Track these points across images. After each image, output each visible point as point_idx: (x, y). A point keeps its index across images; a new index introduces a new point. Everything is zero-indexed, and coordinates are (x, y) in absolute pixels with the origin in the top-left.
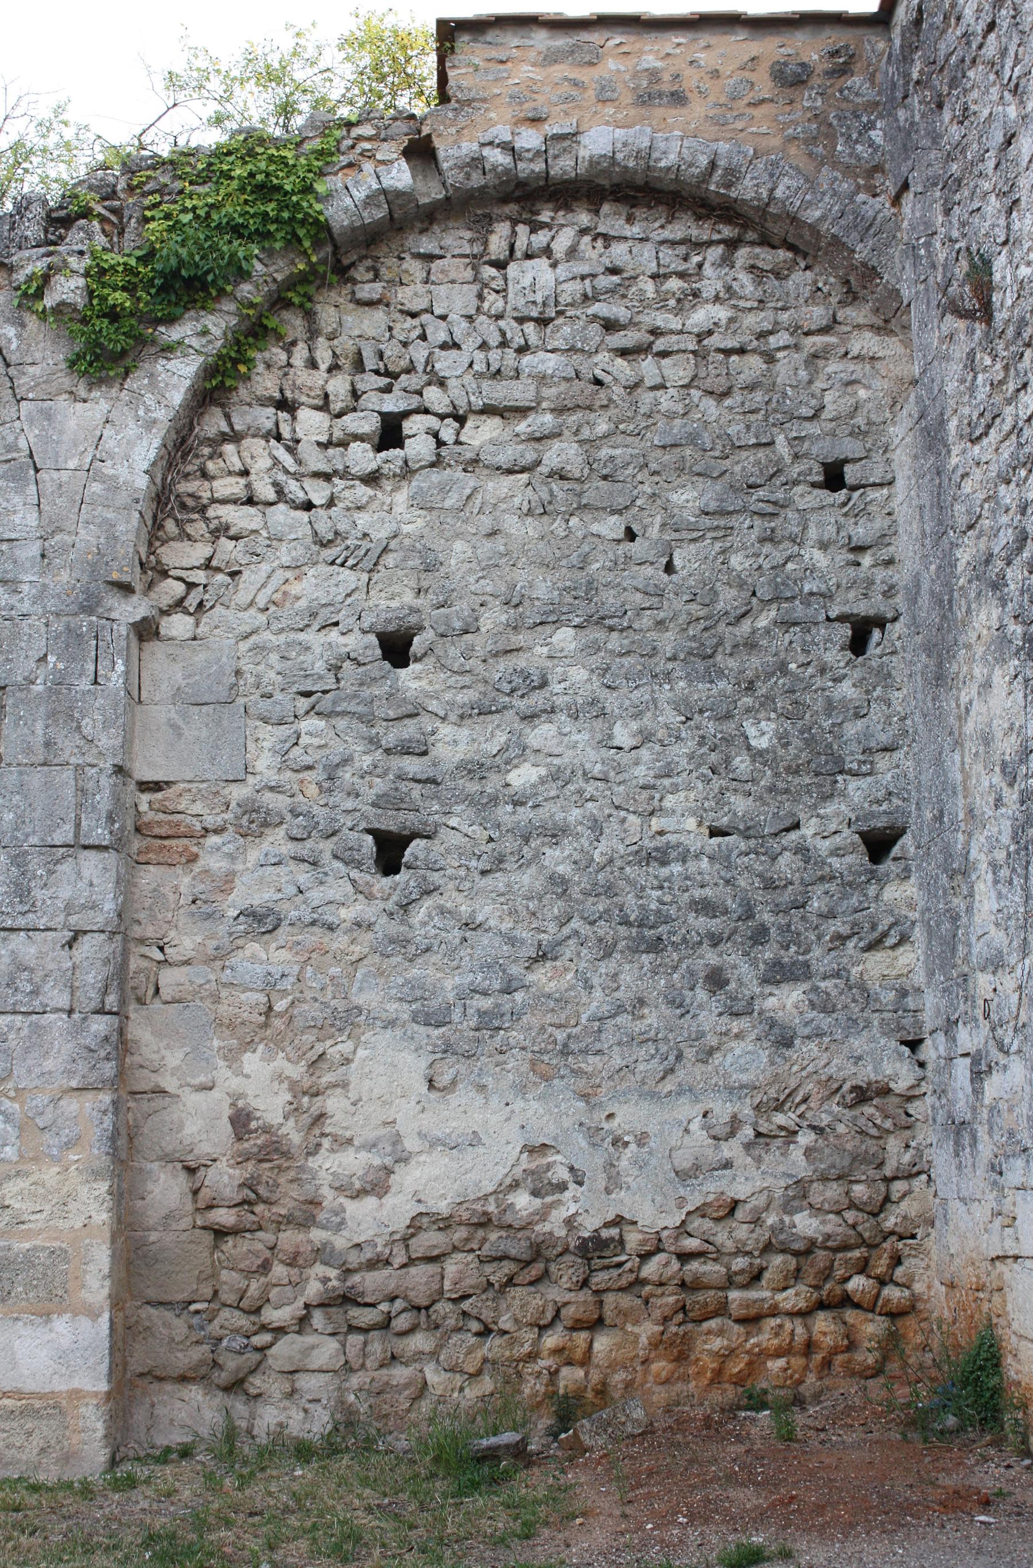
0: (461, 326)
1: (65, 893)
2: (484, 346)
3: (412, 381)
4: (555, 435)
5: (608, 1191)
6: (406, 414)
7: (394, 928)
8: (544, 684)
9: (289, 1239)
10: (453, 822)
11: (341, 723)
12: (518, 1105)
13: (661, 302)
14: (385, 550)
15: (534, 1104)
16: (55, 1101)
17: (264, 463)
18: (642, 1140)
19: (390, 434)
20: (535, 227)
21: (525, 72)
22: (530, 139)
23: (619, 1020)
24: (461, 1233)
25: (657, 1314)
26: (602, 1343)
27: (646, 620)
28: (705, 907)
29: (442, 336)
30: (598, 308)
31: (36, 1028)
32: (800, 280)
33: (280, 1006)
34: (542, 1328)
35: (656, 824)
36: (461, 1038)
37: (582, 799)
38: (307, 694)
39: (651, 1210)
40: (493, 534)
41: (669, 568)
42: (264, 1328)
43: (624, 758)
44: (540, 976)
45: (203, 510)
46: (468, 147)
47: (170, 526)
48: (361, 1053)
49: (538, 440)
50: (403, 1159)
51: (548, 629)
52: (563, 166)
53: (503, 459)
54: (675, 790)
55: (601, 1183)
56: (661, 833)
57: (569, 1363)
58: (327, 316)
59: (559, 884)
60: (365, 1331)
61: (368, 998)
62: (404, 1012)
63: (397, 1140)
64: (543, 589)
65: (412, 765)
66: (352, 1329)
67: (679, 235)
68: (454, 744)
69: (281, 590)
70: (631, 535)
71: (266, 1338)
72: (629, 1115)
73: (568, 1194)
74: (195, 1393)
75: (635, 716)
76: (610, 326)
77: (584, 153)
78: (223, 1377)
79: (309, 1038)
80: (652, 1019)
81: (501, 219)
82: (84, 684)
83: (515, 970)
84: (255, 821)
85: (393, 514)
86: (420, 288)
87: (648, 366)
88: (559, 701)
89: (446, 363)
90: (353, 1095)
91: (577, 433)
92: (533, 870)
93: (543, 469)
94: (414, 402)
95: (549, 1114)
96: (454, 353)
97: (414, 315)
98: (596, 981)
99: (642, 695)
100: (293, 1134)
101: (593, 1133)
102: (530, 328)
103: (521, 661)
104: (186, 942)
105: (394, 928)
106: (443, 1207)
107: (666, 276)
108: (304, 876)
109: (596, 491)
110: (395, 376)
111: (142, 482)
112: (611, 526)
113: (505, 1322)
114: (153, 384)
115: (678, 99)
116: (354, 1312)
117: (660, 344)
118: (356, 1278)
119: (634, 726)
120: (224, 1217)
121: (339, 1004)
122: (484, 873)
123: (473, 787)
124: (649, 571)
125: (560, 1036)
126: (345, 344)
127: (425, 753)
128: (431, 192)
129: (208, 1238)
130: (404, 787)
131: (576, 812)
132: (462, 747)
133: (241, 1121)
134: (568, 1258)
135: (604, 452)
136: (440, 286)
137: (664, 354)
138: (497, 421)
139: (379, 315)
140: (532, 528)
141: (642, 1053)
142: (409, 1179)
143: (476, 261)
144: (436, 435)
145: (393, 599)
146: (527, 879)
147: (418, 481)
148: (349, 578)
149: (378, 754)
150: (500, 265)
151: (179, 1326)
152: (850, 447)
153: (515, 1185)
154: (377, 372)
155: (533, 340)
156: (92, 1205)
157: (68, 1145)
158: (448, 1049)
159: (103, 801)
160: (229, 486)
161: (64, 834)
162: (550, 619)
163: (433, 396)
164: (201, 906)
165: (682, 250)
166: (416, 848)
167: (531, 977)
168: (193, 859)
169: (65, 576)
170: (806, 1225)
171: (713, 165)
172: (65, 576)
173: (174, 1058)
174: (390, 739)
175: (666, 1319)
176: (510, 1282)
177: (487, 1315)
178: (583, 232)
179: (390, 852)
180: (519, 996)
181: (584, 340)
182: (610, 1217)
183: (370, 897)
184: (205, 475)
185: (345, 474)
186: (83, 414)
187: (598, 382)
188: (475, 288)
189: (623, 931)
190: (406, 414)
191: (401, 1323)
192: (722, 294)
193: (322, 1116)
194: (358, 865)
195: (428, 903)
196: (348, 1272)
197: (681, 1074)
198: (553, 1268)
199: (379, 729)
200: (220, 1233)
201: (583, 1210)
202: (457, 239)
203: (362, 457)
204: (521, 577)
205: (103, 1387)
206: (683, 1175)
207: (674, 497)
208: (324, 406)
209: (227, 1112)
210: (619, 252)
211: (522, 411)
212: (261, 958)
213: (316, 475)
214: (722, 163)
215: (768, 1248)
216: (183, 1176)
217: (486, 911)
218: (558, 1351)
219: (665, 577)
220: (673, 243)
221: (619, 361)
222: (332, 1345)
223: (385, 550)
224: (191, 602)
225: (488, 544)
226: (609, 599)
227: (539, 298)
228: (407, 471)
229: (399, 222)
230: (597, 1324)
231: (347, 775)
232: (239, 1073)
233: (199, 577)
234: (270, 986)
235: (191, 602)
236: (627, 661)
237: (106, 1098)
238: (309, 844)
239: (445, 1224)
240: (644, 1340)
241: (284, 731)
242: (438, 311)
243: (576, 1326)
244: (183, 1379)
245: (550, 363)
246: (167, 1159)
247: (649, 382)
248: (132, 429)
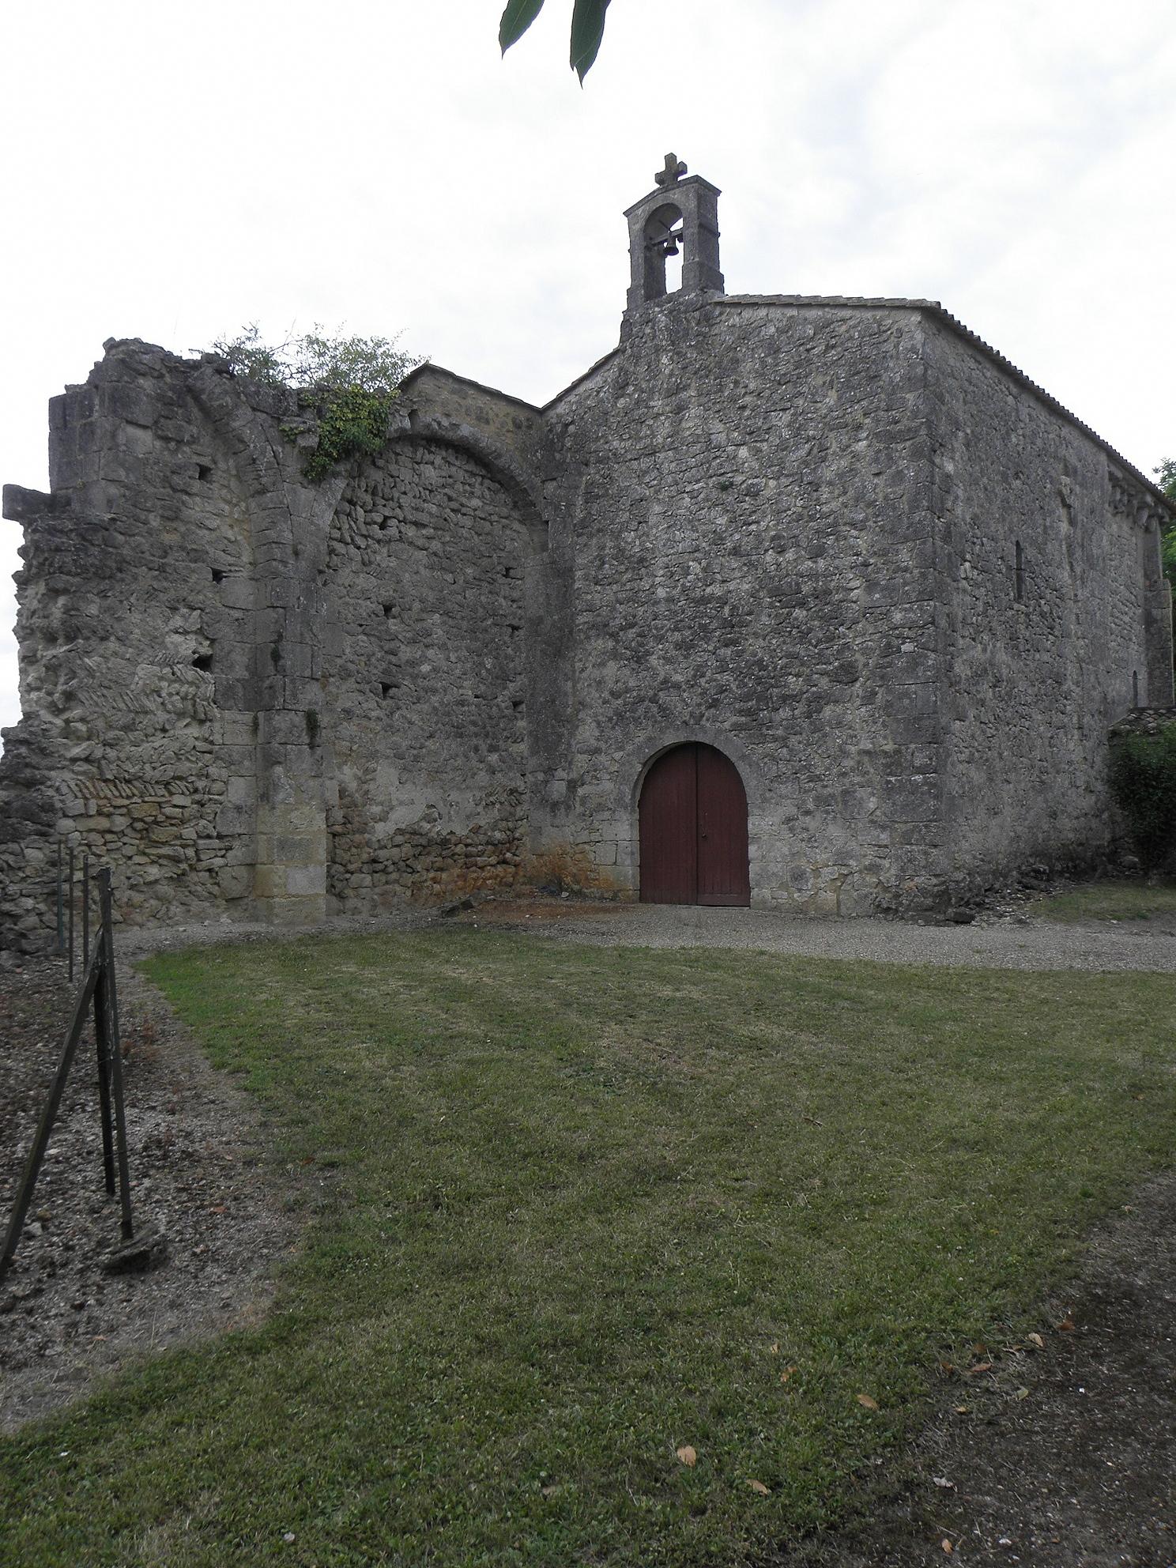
9: (357, 837)
20: (430, 452)
28: (474, 723)
32: (502, 496)
36: (409, 763)
39: (461, 830)
52: (450, 435)
65: (394, 659)
72: (454, 796)
95: (432, 794)
106: (403, 826)
109: (445, 563)
115: (487, 422)
117: (464, 510)
120: (338, 828)
133: (342, 793)
142: (393, 816)
145: (387, 593)
152: (513, 564)
157: (311, 798)
161: (307, 673)
170: (498, 835)
174: (386, 648)
192: (479, 498)
201: (440, 829)
206: (468, 817)
211: (424, 526)
215: (488, 843)
217: (415, 718)
229: (404, 437)
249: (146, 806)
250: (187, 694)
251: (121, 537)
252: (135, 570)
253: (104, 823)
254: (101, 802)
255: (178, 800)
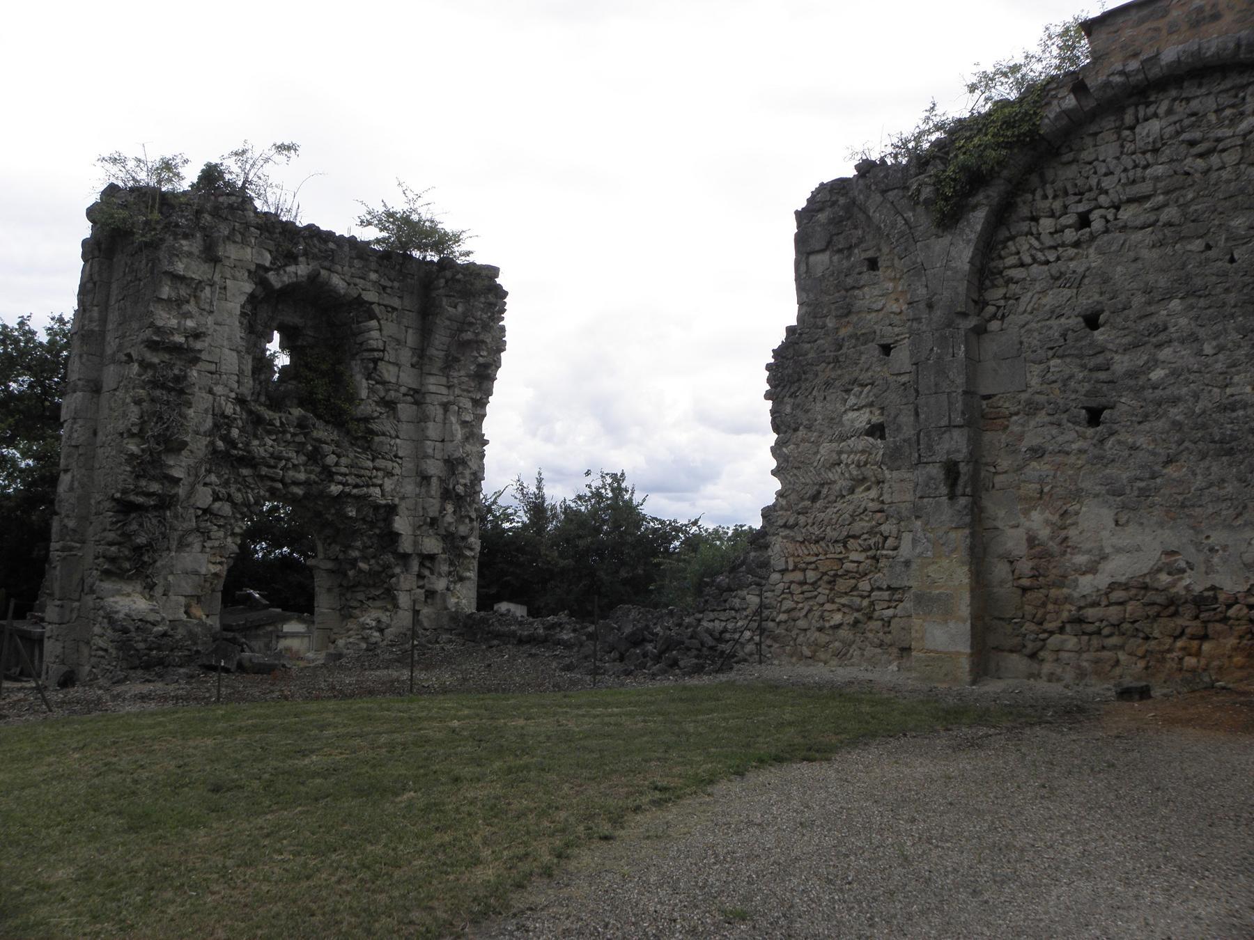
0: (1112, 163)
1: (946, 446)
2: (1125, 170)
3: (1092, 194)
4: (1165, 205)
5: (1207, 573)
6: (1090, 211)
7: (1097, 452)
8: (1165, 329)
9: (1054, 592)
10: (1123, 400)
11: (1068, 360)
12: (1159, 531)
13: (1220, 123)
14: (1084, 277)
15: (1167, 531)
16: (947, 533)
17: (1026, 247)
18: (1225, 548)
19: (1084, 221)
20: (1148, 105)
21: (1128, 33)
22: (1133, 65)
23: (1211, 490)
24: (1133, 592)
25: (1236, 634)
26: (1206, 647)
27: (1219, 289)
29: (1104, 170)
30: (1185, 136)
31: (937, 503)
33: (1046, 489)
34: (1176, 638)
35: (1229, 391)
36: (1130, 502)
37: (1187, 382)
38: (1052, 348)
40: (1136, 260)
41: (1232, 260)
42: (1045, 631)
43: (1210, 360)
44: (1169, 470)
45: (1001, 273)
46: (1101, 79)
47: (987, 283)
48: (1084, 509)
49: (1157, 209)
50: (1104, 558)
51: (1166, 302)
52: (1155, 72)
53: (1138, 223)
54: (1238, 373)
55: (1203, 569)
56: (1232, 395)
57: (1190, 655)
58: (1050, 174)
59: (1177, 425)
60: (1090, 634)
61: (1086, 485)
62: (1103, 489)
63: (1101, 549)
64: (1163, 282)
65: (1102, 376)
66: (1084, 633)
67: (1229, 86)
68: (1122, 363)
69: (1038, 301)
70: (1208, 247)
71: (1046, 635)
72: (1218, 537)
73: (1186, 575)
74: (1015, 656)
75: (1215, 339)
76: (1192, 143)
77: (1163, 63)
78: (1028, 651)
79: (1060, 503)
80: (1229, 488)
81: (1129, 106)
82: (949, 358)
83: (1157, 468)
84: (1032, 409)
85: (1093, 258)
86: (1092, 150)
87: (1215, 160)
88: (1174, 336)
89: (1105, 184)
90: (1080, 528)
91: (1177, 201)
92: (1164, 419)
93: (1160, 223)
94: (1093, 204)
96: (1110, 177)
97: (1090, 163)
98: (1198, 471)
99: (1219, 327)
100: (1053, 546)
101: (1198, 546)
102: (1148, 156)
103: (1154, 320)
104: (1004, 463)
105: (1097, 452)
106: (1123, 579)
107: (1223, 109)
108: (1054, 431)
110: (1082, 194)
111: (967, 267)
112: (1197, 245)
113: (1156, 633)
114: (969, 223)
116: (1084, 626)
117: (1220, 146)
118: (1084, 611)
119: (1214, 343)
120: (1025, 582)
121: (1073, 488)
122: (1140, 423)
123: (1132, 383)
124: (1219, 264)
125: (1180, 498)
126: (1059, 184)
127: (1108, 369)
128: (1090, 104)
129: (1020, 592)
130: (1098, 386)
131: (1185, 390)
132: (1126, 364)
133: (1032, 541)
134: (1188, 605)
135: (1193, 208)
136: (1104, 148)
137: (1224, 150)
138: (1136, 205)
139: (1074, 167)
140: (1155, 253)
141: (1224, 505)
143: (1118, 130)
144: (1105, 217)
145: (1089, 299)
146: (1160, 424)
147: (1098, 242)
148: (1067, 293)
149: (1086, 373)
150: (1132, 128)
151: (1009, 629)
153: (1159, 570)
154: (1075, 194)
155: (1151, 161)
156: (962, 576)
157: (953, 551)
158: (1124, 507)
159: (959, 406)
160: (1012, 260)
161: (944, 422)
162: (1167, 297)
163: (1103, 199)
164: (1012, 449)
165: (1233, 92)
166: (1106, 413)
167: (1165, 471)
168: (1007, 427)
169: (939, 313)
171: (1238, 45)
172: (939, 313)
173: (1002, 514)
174: (1091, 364)
175: (1241, 637)
176: (1158, 615)
177: (1147, 630)
178: (1174, 100)
179: (1094, 416)
180: (1158, 480)
181: (1178, 154)
182: (1208, 586)
183: (1085, 438)
184: (1001, 258)
185: (1063, 245)
186: (940, 244)
187: (1187, 174)
188: (1118, 143)
189: (1212, 446)
190: (1090, 211)
191: (1106, 631)
193: (1066, 539)
194: (1078, 424)
195: (1113, 439)
196: (1080, 608)
197: (1246, 516)
198: (1181, 609)
199: (1086, 361)
200: (1025, 590)
201: (1194, 582)
202: (1109, 122)
203: (1070, 235)
204: (1151, 278)
205: (968, 651)
207: (1232, 223)
208: (1052, 215)
209: (1025, 537)
210: (1195, 105)
211: (1147, 198)
212: (1037, 468)
213: (1051, 248)
214: (1244, 42)
216: (1008, 565)
217: (1142, 441)
218: (1183, 649)
219: (1229, 266)
220: (1226, 91)
221: (1199, 161)
222: (1075, 640)
223: (1084, 277)
224: (1000, 314)
225: (1134, 265)
226: (1198, 282)
227: (1151, 139)
228: (1093, 238)
230: (1205, 638)
231: (1072, 384)
232: (1029, 520)
233: (1002, 303)
234: (1041, 481)
235: (1000, 314)
236: (1209, 311)
237: (967, 531)
238: (1057, 416)
239: (1126, 587)
240: (1229, 646)
241: (1043, 366)
242: (1101, 159)
243: (1193, 638)
244: (1011, 651)
245: (1159, 170)
246: (1001, 557)
247: (1215, 167)
248: (961, 245)
249: (828, 562)
250: (859, 461)
251: (809, 346)
252: (815, 368)
253: (798, 576)
254: (797, 560)
255: (854, 556)
